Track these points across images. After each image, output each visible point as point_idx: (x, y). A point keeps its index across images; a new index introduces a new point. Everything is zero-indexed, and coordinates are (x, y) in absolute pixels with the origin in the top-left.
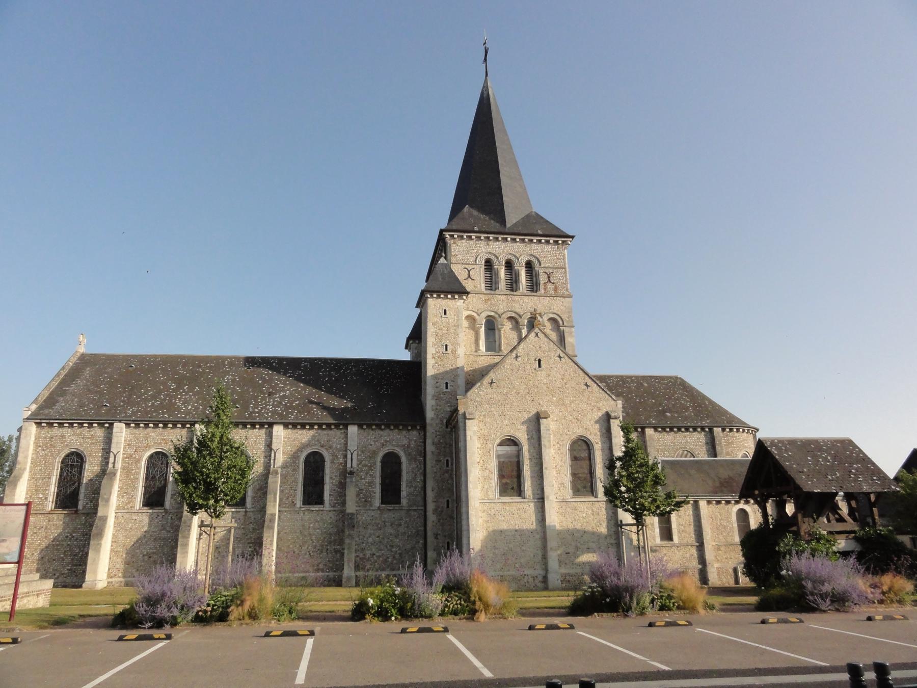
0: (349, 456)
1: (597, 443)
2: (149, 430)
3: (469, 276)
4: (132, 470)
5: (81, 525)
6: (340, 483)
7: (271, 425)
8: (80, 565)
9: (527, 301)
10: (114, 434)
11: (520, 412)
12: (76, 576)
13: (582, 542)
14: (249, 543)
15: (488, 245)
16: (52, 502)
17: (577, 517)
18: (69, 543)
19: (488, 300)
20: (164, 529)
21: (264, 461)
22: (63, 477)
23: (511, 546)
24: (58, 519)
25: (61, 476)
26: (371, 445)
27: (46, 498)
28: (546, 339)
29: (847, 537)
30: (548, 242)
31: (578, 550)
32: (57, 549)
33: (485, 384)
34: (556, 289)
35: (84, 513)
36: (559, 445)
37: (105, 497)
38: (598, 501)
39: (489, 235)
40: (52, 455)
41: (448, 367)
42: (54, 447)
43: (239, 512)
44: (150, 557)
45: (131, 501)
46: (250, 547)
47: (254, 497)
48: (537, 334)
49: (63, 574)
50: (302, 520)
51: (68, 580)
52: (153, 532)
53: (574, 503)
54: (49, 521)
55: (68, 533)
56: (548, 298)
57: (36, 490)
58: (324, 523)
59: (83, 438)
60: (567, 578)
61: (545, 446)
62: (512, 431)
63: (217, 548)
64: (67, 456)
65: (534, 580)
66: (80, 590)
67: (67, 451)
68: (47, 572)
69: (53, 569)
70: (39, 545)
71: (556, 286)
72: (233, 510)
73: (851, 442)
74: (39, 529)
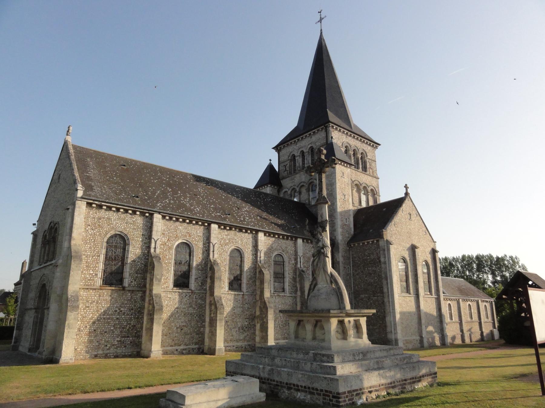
0: (299, 259)
2: (178, 223)
4: (167, 255)
5: (127, 301)
6: (293, 277)
7: (257, 231)
8: (128, 337)
10: (154, 223)
12: (125, 347)
14: (245, 319)
16: (101, 279)
18: (118, 317)
20: (191, 306)
21: (252, 257)
22: (108, 257)
24: (107, 294)
25: (106, 255)
26: (307, 253)
27: (96, 275)
32: (109, 323)
35: (129, 291)
37: (158, 277)
40: (100, 235)
41: (346, 209)
42: (102, 228)
43: (240, 294)
44: (182, 329)
45: (166, 282)
46: (246, 321)
47: (248, 284)
49: (113, 345)
50: (275, 303)
51: (119, 351)
52: (183, 308)
54: (100, 296)
55: (116, 307)
57: (87, 266)
58: (286, 305)
59: (127, 223)
63: (226, 322)
64: (112, 237)
66: (149, 359)
67: (112, 233)
68: (100, 344)
69: (105, 341)
70: (92, 317)
72: (236, 293)
73: (536, 274)
74: (91, 303)
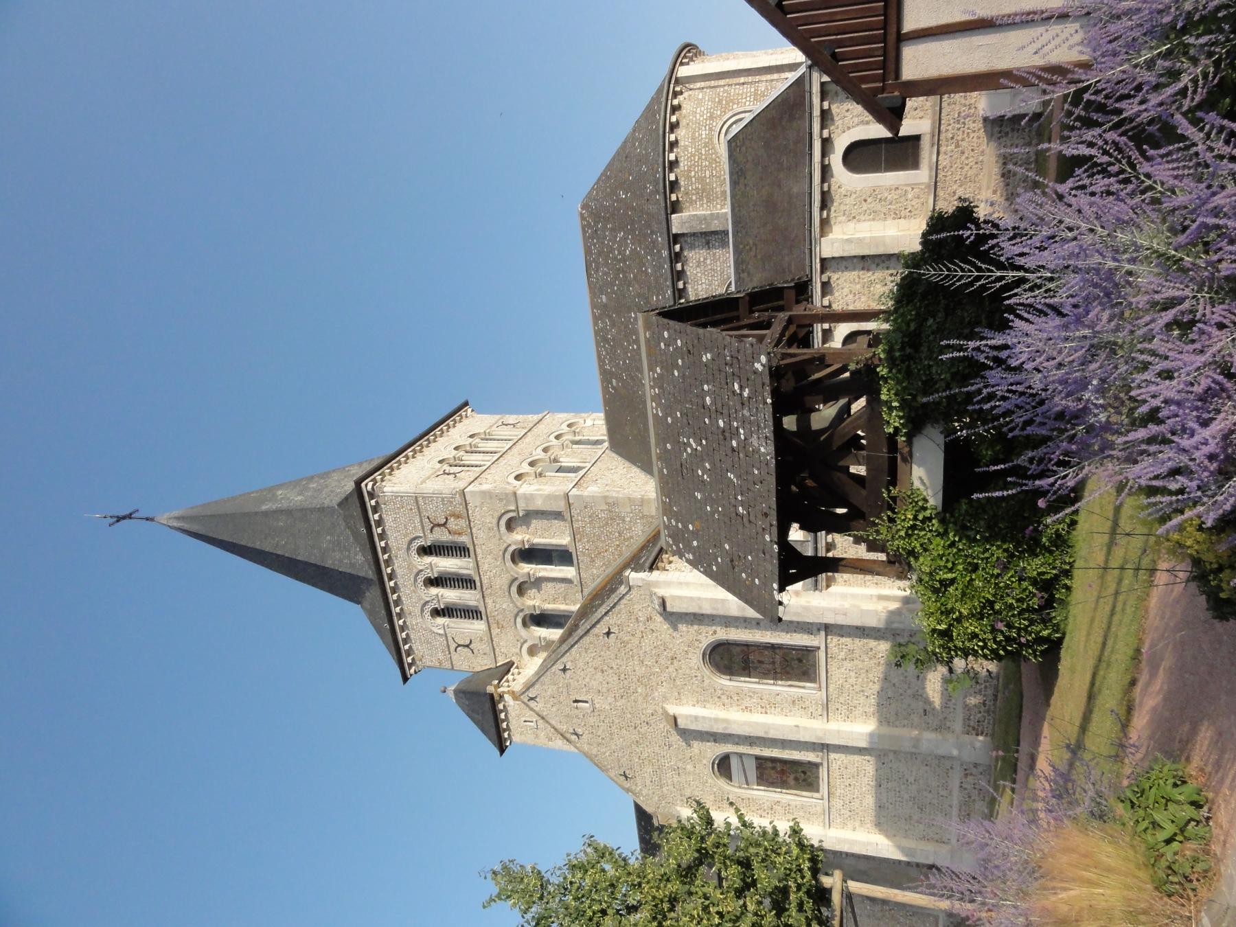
1: (715, 632)
3: (467, 646)
9: (487, 566)
11: (670, 746)
13: (906, 686)
15: (410, 614)
17: (858, 688)
19: (498, 623)
23: (906, 796)
28: (537, 686)
29: (905, 460)
30: (379, 523)
31: (920, 695)
33: (629, 785)
34: (458, 517)
36: (723, 697)
38: (826, 647)
39: (394, 614)
48: (532, 699)
53: (831, 689)
56: (474, 530)
60: (972, 723)
61: (726, 728)
62: (705, 762)
65: (971, 774)
71: (451, 516)
